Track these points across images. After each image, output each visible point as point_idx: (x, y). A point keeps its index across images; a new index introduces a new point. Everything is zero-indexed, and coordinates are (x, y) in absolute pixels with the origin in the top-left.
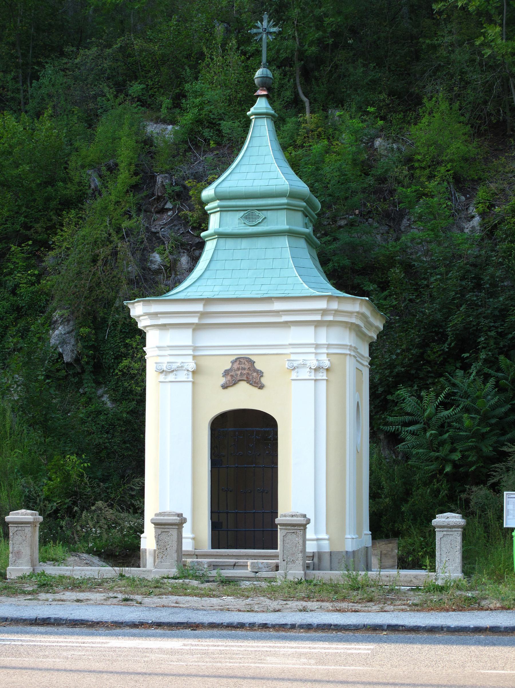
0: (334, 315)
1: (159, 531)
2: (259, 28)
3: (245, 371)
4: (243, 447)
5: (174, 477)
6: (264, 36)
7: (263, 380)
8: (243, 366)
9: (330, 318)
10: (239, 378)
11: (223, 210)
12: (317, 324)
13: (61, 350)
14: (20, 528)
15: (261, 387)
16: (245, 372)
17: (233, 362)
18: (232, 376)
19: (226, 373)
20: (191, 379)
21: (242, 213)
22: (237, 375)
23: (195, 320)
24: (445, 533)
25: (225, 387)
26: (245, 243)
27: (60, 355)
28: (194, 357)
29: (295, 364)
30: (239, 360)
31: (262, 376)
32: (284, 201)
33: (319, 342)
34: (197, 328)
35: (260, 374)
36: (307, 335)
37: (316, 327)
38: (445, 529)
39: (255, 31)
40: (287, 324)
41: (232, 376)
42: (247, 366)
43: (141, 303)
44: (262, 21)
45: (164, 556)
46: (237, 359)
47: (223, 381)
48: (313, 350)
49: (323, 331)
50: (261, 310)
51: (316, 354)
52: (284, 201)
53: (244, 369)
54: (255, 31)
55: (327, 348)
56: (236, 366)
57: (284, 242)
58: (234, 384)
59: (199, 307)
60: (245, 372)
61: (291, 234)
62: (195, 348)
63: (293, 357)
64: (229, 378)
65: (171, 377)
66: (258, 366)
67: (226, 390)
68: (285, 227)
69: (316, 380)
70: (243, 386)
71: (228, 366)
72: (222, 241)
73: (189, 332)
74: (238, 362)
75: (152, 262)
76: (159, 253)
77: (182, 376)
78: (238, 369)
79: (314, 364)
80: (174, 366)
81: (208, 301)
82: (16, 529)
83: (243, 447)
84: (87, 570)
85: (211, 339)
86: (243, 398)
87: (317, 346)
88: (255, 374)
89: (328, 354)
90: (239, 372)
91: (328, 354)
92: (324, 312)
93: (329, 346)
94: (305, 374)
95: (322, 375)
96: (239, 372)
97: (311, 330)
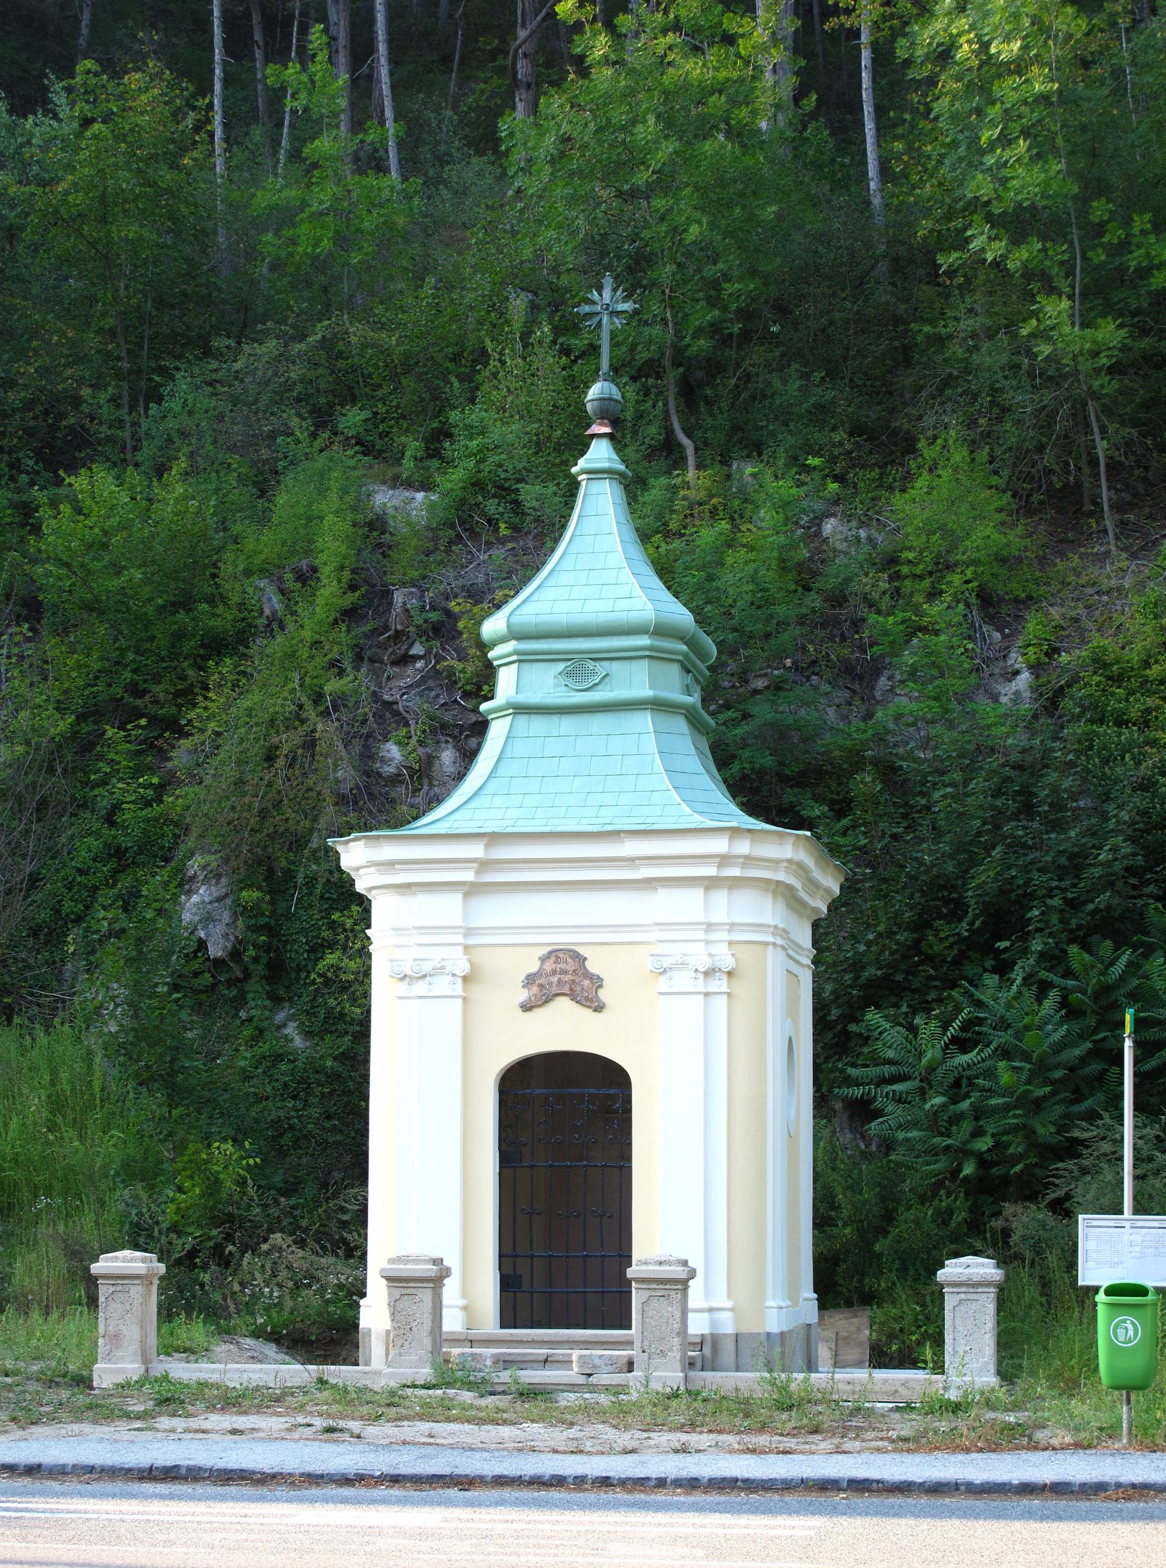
0: (743, 866)
1: (397, 1293)
2: (594, 303)
3: (567, 977)
4: (564, 1129)
5: (429, 1188)
6: (605, 319)
7: (603, 995)
8: (563, 966)
9: (736, 872)
10: (554, 990)
11: (524, 659)
12: (710, 884)
13: (202, 935)
14: (119, 1288)
15: (599, 1008)
16: (566, 978)
17: (543, 959)
18: (541, 986)
19: (530, 980)
20: (459, 992)
21: (561, 666)
22: (550, 984)
23: (469, 876)
24: (963, 1296)
25: (527, 1007)
26: (566, 724)
27: (202, 945)
28: (467, 948)
29: (667, 963)
30: (554, 954)
31: (601, 986)
32: (644, 641)
33: (713, 920)
34: (471, 890)
35: (597, 982)
36: (689, 904)
37: (707, 889)
38: (964, 1289)
39: (586, 308)
40: (649, 884)
41: (541, 986)
42: (571, 966)
43: (362, 843)
44: (600, 290)
45: (406, 1344)
46: (550, 953)
47: (523, 995)
48: (701, 935)
49: (721, 897)
50: (595, 854)
51: (707, 942)
52: (644, 641)
53: (566, 972)
54: (586, 308)
55: (707, 931)
56: (549, 966)
57: (645, 721)
58: (546, 1002)
59: (476, 850)
60: (566, 978)
61: (658, 706)
62: (469, 932)
63: (660, 949)
64: (535, 989)
65: (420, 988)
66: (592, 967)
67: (528, 1014)
68: (646, 692)
69: (707, 994)
70: (563, 1004)
71: (534, 967)
72: (522, 720)
73: (456, 899)
74: (553, 959)
75: (383, 760)
76: (398, 743)
77: (442, 985)
78: (554, 972)
79: (704, 963)
80: (427, 967)
81: (493, 838)
82: (112, 1289)
83: (564, 1129)
84: (255, 1371)
85: (495, 912)
86: (562, 1030)
87: (710, 927)
88: (586, 982)
89: (730, 943)
90: (555, 979)
91: (730, 943)
92: (724, 860)
93: (732, 927)
94: (684, 980)
95: (720, 984)
96: (555, 979)
97: (696, 895)
